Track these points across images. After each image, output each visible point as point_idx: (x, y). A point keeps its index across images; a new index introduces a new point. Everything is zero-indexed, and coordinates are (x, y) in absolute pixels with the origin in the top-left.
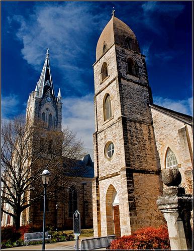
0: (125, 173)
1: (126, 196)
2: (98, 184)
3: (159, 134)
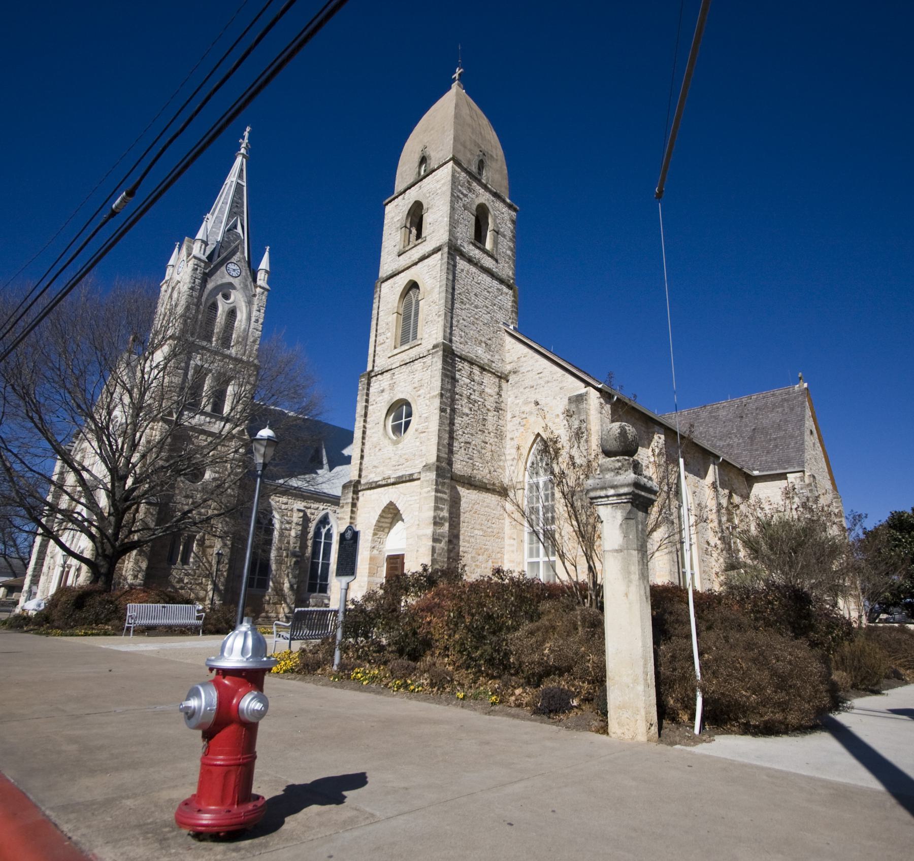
0: (433, 475)
1: (429, 530)
2: (358, 499)
3: (520, 401)
